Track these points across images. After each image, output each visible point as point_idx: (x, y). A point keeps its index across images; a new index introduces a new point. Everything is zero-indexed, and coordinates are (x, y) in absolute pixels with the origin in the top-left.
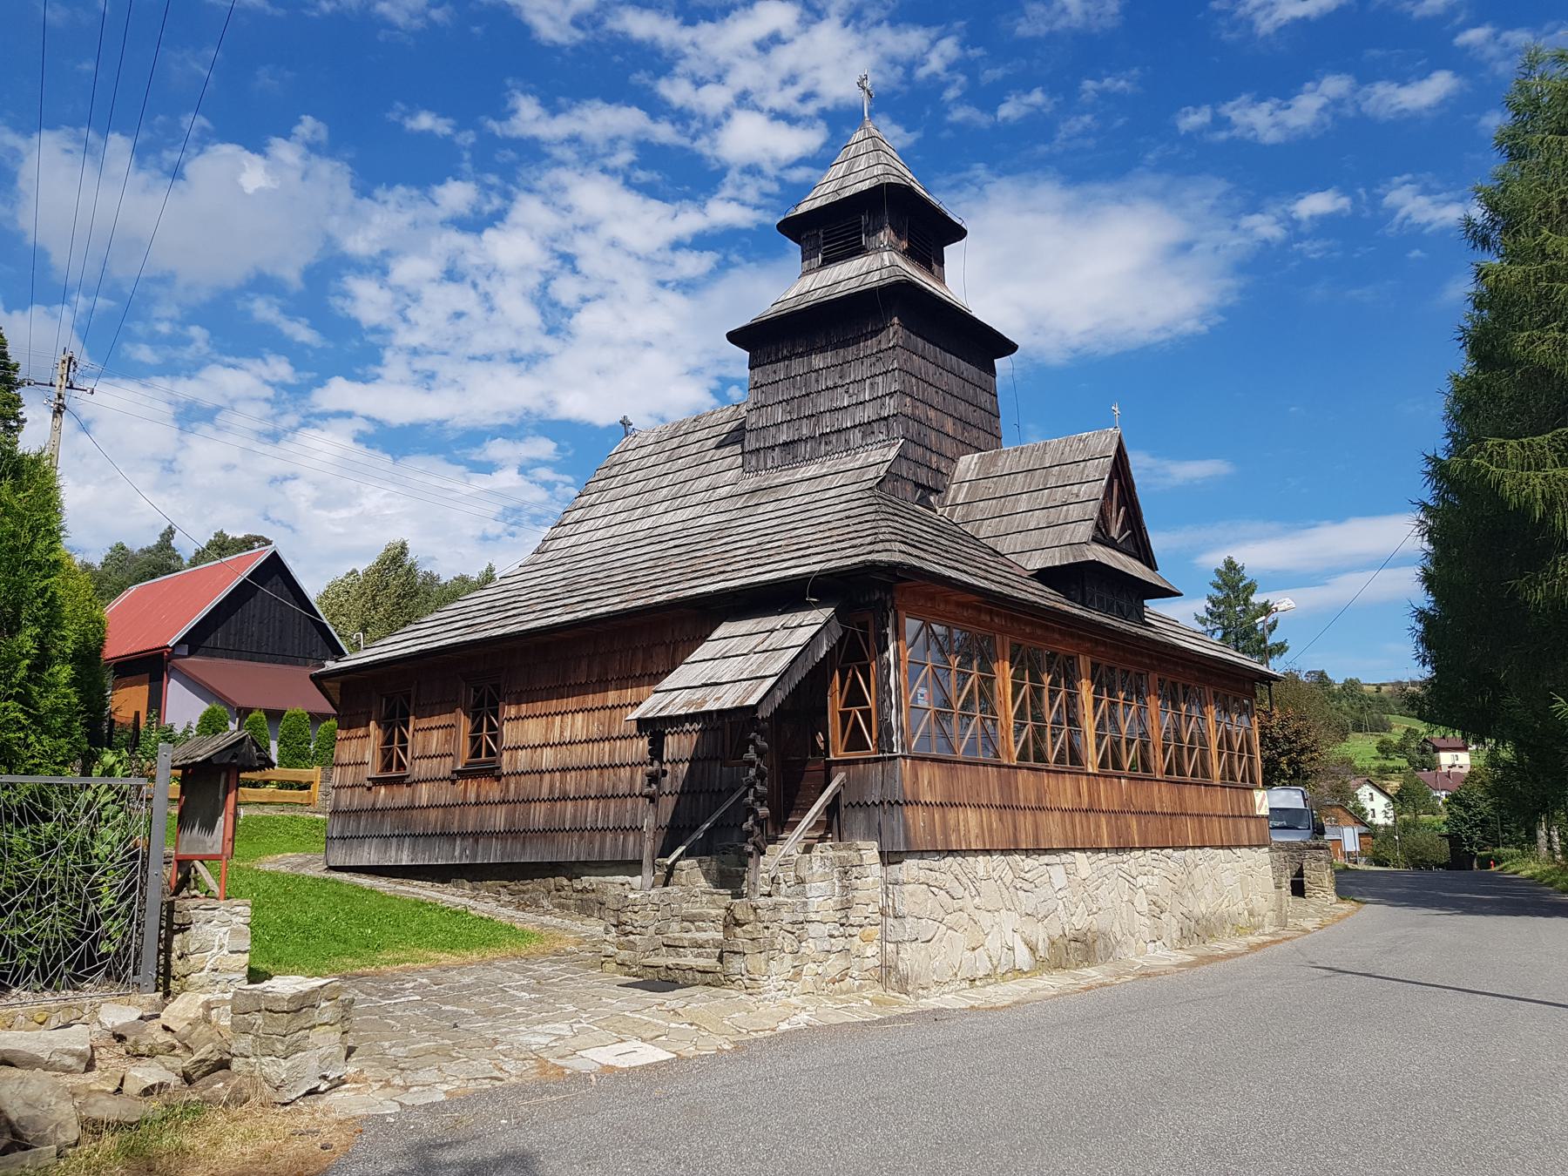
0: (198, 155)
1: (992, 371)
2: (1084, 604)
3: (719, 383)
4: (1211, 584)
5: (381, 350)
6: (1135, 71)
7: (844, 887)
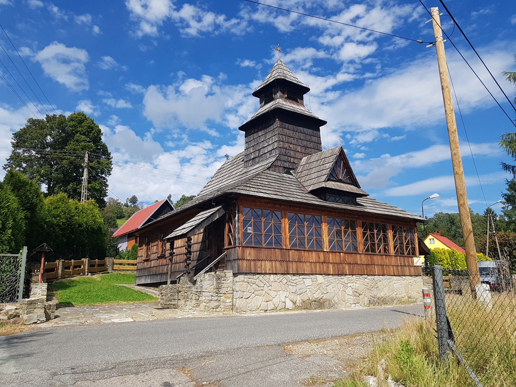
0: (183, 83)
1: (319, 130)
2: (325, 200)
3: (343, 134)
4: (506, 189)
5: (236, 136)
6: (493, 5)
7: (217, 283)
